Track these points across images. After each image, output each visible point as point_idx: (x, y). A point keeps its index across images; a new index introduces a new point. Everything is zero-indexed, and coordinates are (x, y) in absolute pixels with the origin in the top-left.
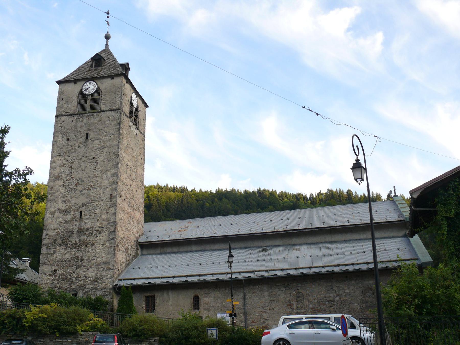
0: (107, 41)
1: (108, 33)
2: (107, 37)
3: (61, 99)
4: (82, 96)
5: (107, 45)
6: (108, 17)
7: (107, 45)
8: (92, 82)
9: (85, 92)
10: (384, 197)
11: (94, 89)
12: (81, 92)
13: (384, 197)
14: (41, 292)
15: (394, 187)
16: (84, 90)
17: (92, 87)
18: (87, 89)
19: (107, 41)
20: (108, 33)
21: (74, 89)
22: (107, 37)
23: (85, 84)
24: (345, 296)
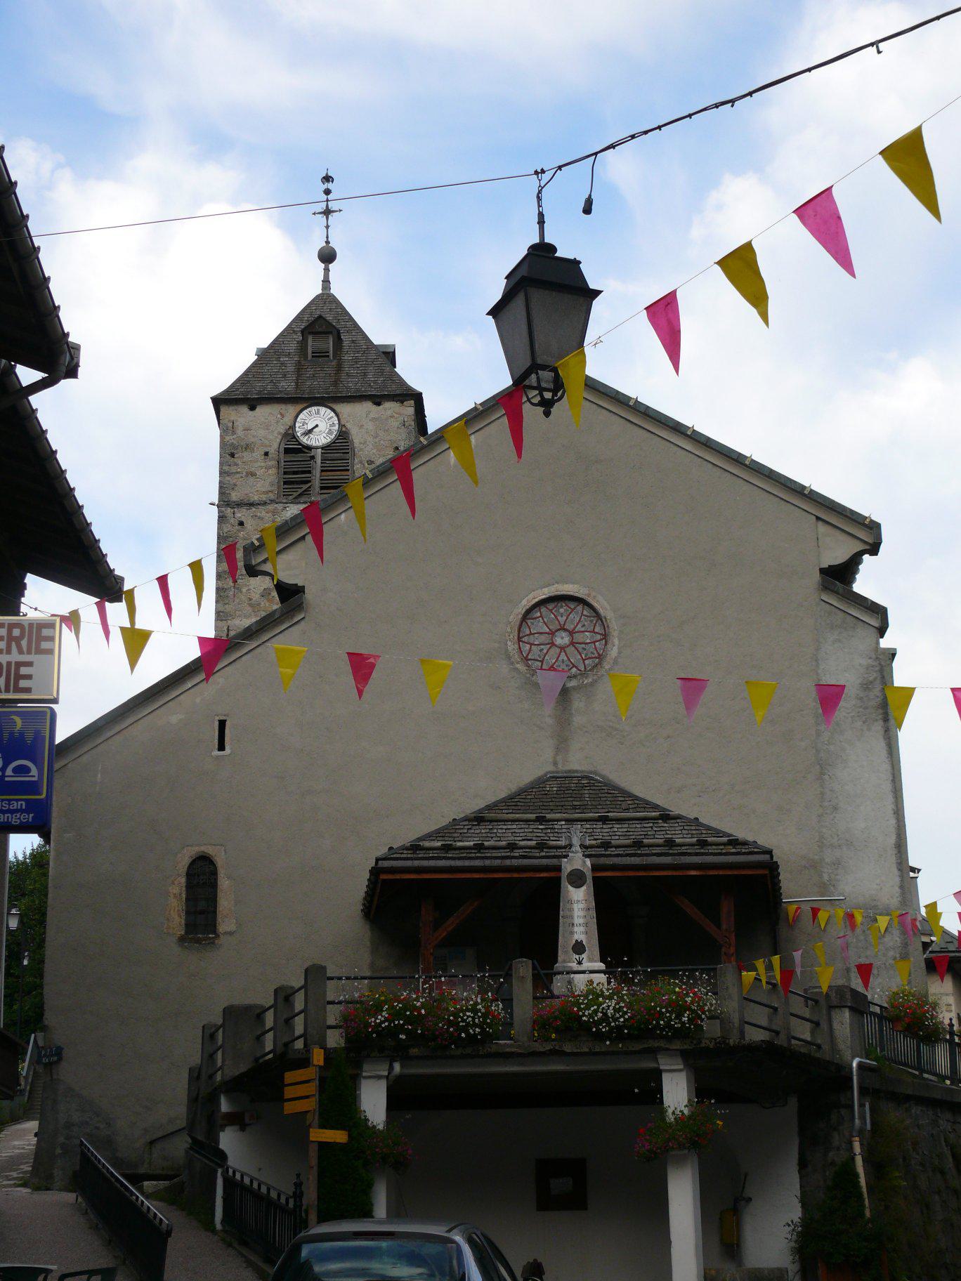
0: (327, 270)
1: (327, 242)
2: (327, 256)
3: (229, 453)
4: (294, 449)
5: (326, 282)
6: (327, 192)
7: (326, 282)
8: (323, 410)
9: (305, 440)
10: (884, 643)
11: (330, 432)
12: (290, 435)
13: (884, 643)
14: (870, 661)
15: (222, 724)
16: (299, 432)
17: (323, 426)
18: (310, 431)
19: (327, 270)
20: (327, 242)
21: (265, 424)
22: (327, 256)
23: (301, 416)
24: (621, 999)
